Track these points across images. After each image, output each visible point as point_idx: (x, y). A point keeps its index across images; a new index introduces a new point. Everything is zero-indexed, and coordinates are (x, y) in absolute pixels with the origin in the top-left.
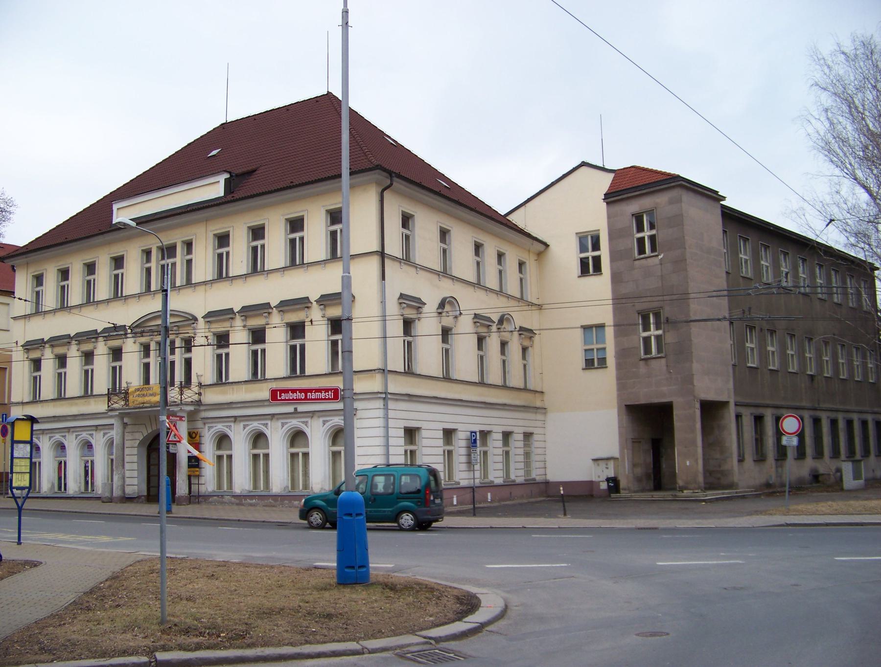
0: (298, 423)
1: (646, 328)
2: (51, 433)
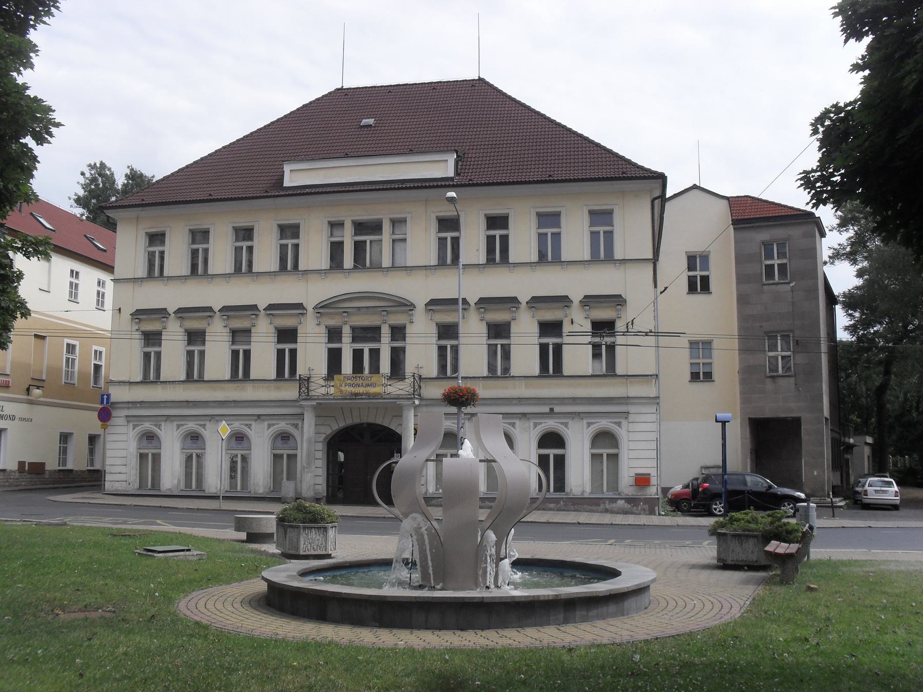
0: (610, 424)
1: (773, 348)
2: (270, 419)
